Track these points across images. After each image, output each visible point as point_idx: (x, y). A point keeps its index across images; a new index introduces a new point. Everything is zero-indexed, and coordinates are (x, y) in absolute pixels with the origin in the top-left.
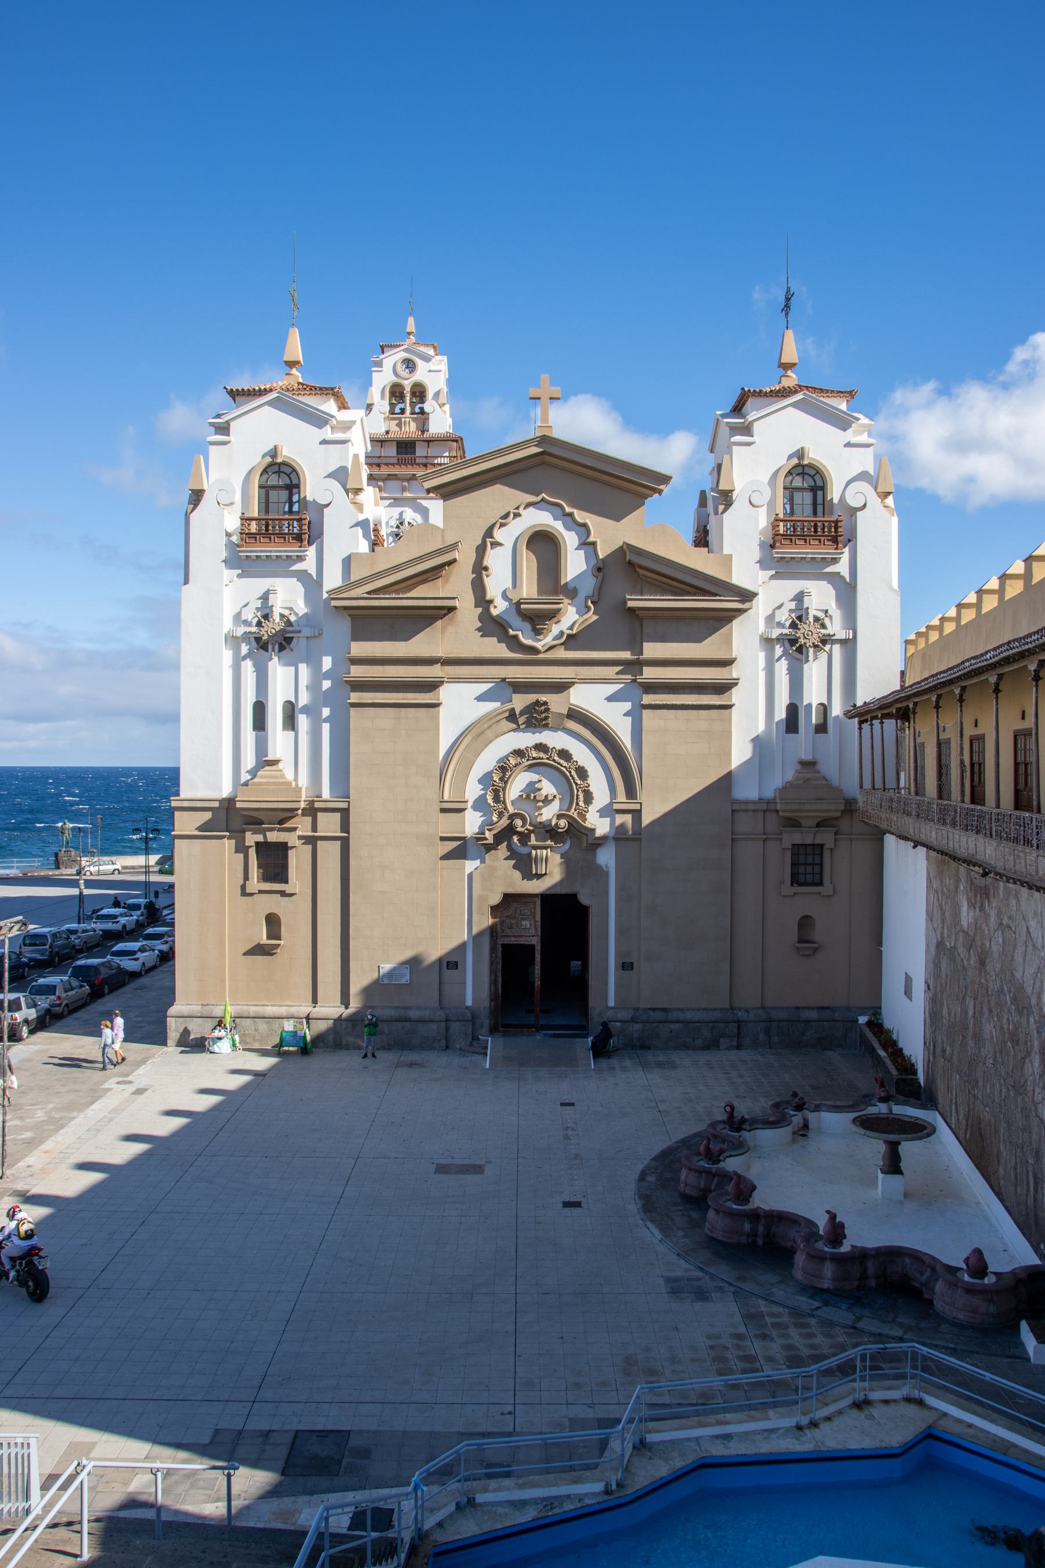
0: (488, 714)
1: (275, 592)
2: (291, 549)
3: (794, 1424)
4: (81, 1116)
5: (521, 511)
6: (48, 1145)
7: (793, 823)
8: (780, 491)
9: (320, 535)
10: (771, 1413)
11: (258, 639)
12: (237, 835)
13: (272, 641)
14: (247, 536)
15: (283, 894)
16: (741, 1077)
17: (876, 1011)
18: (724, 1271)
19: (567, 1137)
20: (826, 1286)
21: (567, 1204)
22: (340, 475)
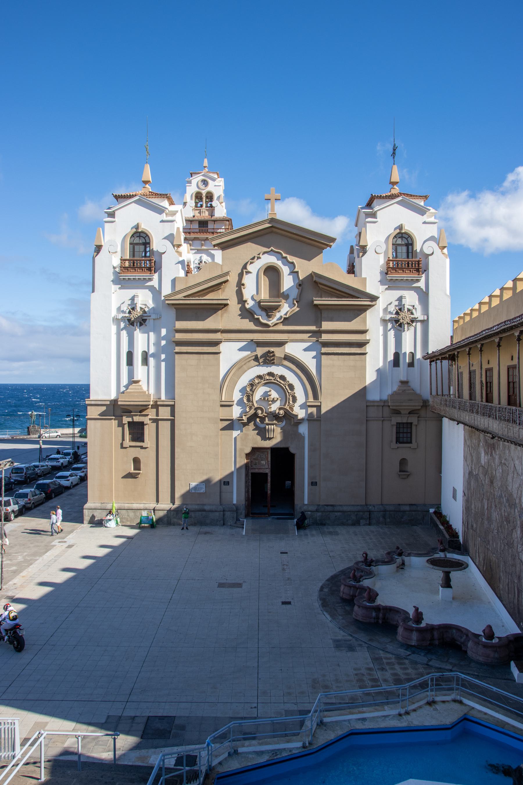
0: (244, 357)
1: (138, 296)
2: (146, 275)
3: (397, 713)
4: (41, 559)
5: (261, 256)
6: (24, 573)
7: (397, 412)
8: (390, 246)
9: (160, 268)
10: (386, 707)
11: (129, 320)
12: (119, 418)
13: (136, 321)
14: (124, 268)
15: (142, 447)
16: (371, 539)
17: (438, 506)
18: (362, 636)
19: (284, 569)
20: (413, 644)
21: (284, 603)
22: (170, 238)
